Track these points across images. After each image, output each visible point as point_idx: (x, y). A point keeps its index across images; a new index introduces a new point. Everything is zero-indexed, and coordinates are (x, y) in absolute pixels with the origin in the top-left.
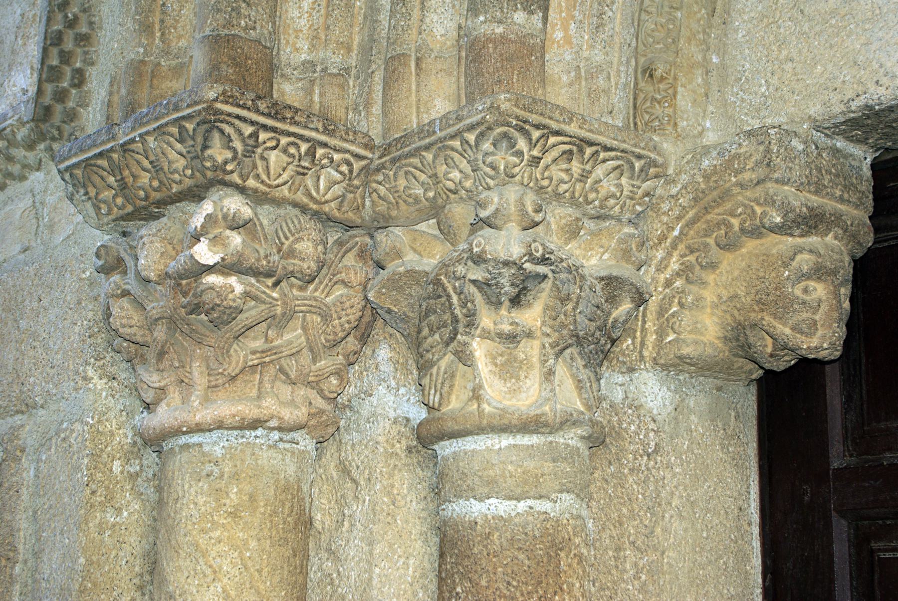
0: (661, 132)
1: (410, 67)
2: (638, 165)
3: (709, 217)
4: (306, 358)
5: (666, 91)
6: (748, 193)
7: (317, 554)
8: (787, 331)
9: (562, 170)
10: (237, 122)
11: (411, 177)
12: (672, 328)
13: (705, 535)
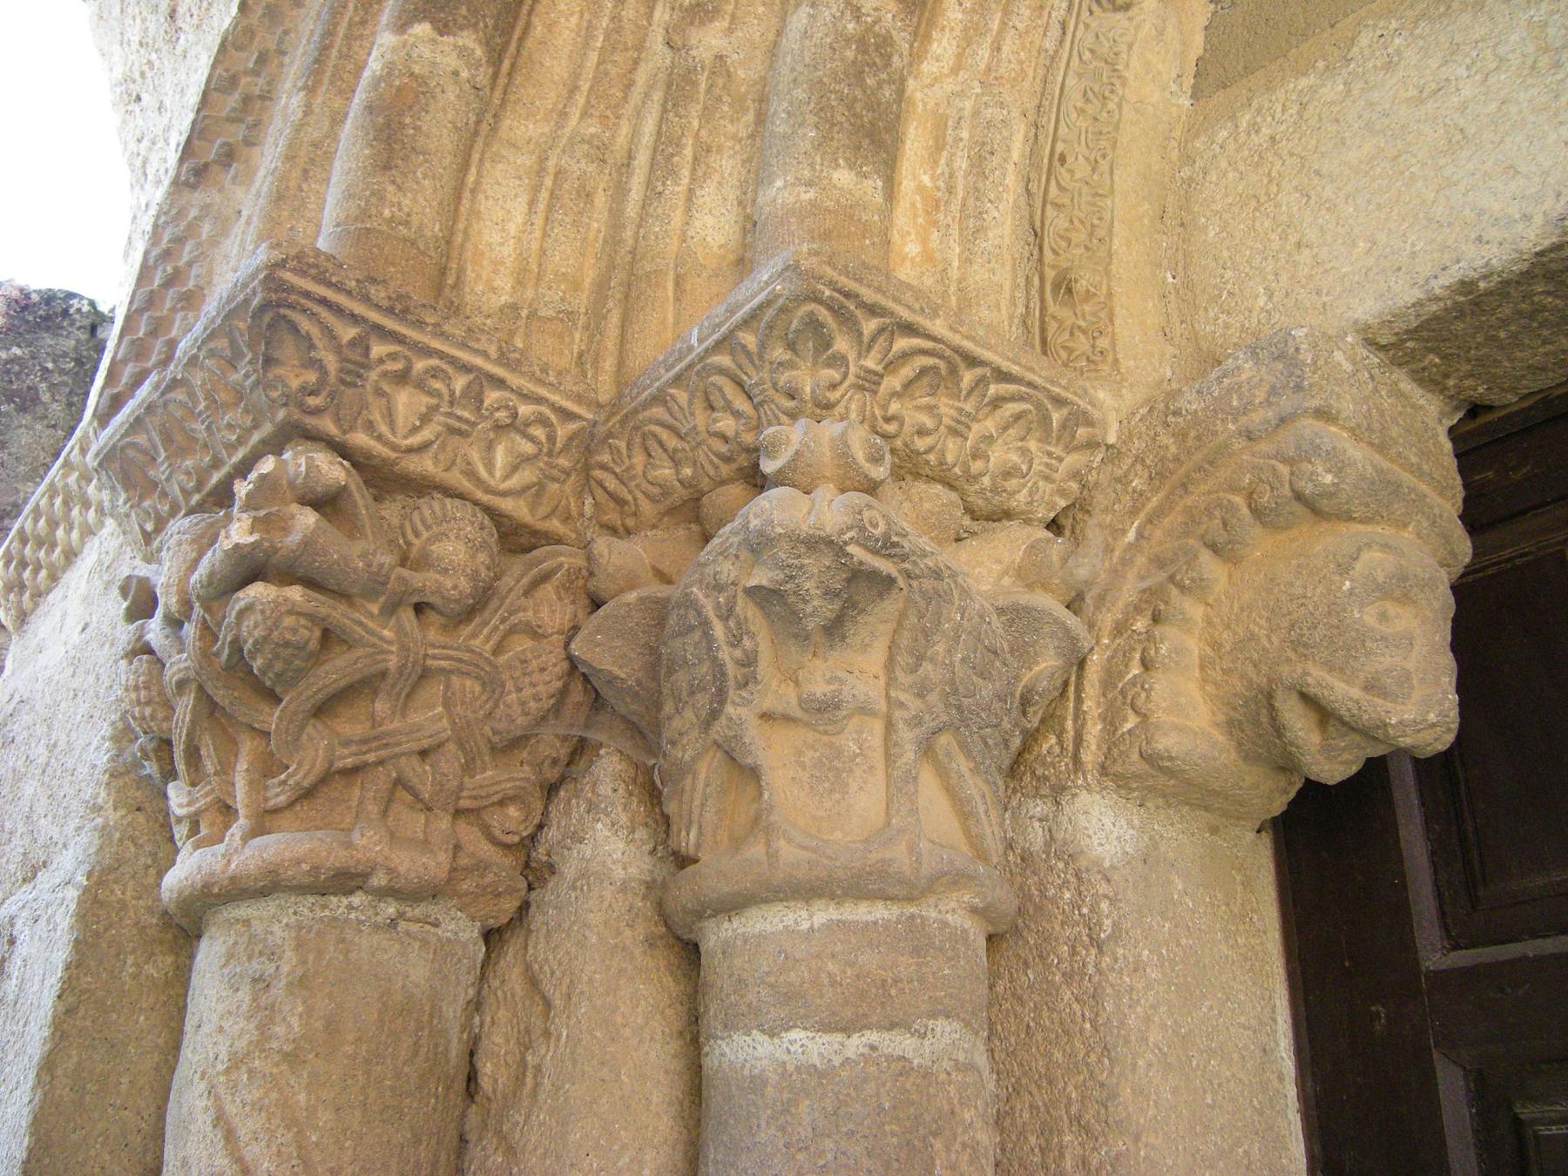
0: (1094, 375)
1: (665, 288)
2: (1056, 417)
3: (1189, 501)
4: (450, 761)
5: (1095, 314)
6: (1264, 447)
7: (480, 1140)
8: (1356, 693)
9: (918, 408)
10: (324, 314)
11: (656, 446)
12: (1133, 706)
13: (1209, 1101)
